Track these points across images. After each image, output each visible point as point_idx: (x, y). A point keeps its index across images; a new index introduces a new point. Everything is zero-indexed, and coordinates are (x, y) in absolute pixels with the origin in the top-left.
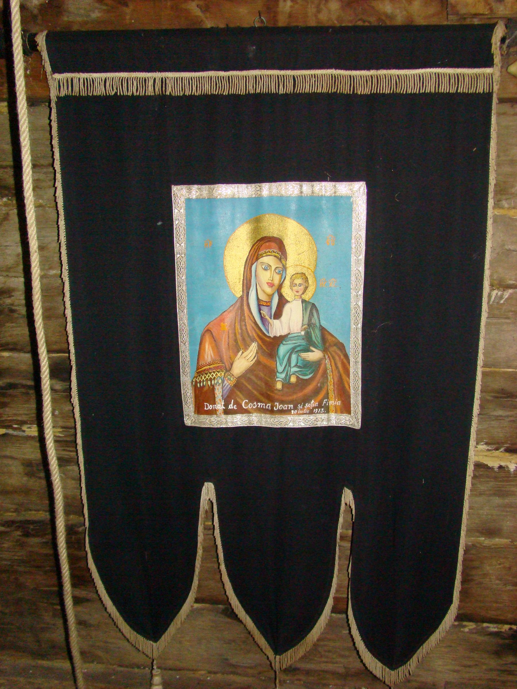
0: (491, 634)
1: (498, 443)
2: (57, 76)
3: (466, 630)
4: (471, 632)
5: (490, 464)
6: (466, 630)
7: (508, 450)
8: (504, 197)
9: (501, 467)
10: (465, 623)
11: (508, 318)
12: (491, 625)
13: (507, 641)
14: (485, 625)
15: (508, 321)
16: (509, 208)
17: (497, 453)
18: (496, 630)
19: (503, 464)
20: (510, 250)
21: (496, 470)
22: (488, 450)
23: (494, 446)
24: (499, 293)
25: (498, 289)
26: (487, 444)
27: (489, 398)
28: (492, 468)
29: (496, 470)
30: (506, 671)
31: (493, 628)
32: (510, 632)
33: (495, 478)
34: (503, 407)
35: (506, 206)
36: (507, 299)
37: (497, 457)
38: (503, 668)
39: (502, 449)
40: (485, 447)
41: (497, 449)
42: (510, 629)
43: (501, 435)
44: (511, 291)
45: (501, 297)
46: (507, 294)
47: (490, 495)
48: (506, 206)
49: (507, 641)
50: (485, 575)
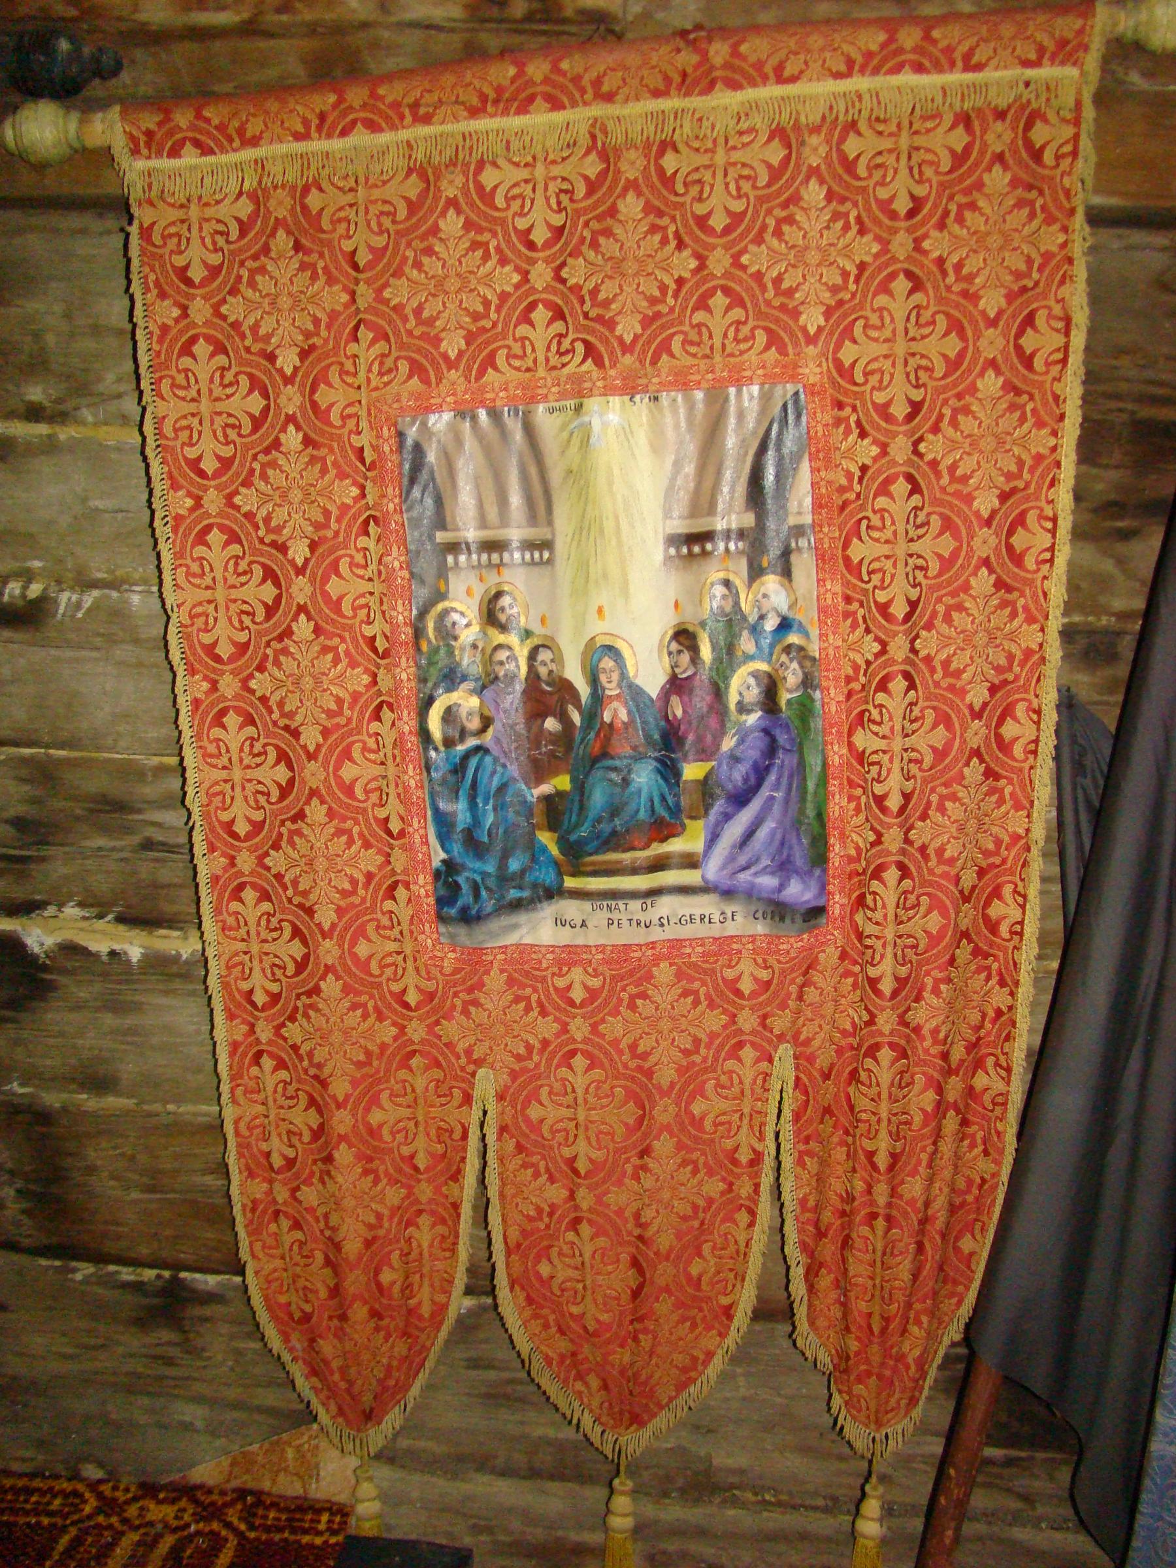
0: (125, 1285)
1: (99, 905)
2: (141, 164)
3: (79, 1276)
4: (87, 1281)
5: (93, 947)
6: (79, 1276)
7: (121, 919)
8: (84, 401)
9: (113, 953)
10: (74, 1264)
11: (97, 649)
12: (124, 1270)
13: (156, 1301)
14: (112, 1268)
15: (95, 654)
16: (95, 424)
17: (100, 924)
18: (132, 1278)
19: (117, 947)
20: (97, 509)
21: (105, 958)
22: (84, 918)
23: (94, 911)
24: (74, 598)
25: (72, 589)
26: (81, 905)
27: (78, 812)
28: (95, 956)
29: (105, 958)
30: (162, 1357)
31: (127, 1274)
32: (159, 1283)
33: (105, 975)
34: (105, 830)
35: (90, 419)
36: (89, 610)
37: (104, 933)
38: (153, 1352)
39: (110, 917)
40: (76, 912)
41: (101, 916)
42: (159, 1277)
43: (104, 887)
44: (96, 593)
45: (78, 606)
46: (88, 600)
47: (98, 1009)
48: (90, 419)
49: (156, 1301)
50: (91, 1170)
